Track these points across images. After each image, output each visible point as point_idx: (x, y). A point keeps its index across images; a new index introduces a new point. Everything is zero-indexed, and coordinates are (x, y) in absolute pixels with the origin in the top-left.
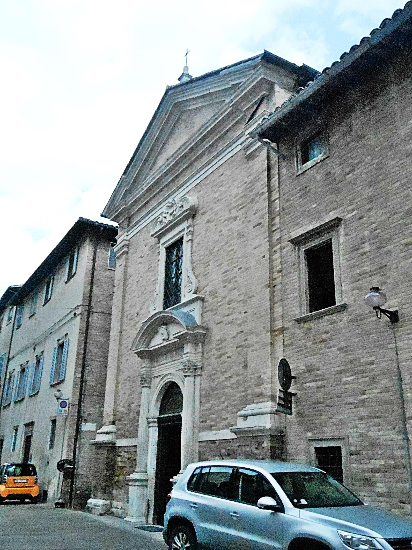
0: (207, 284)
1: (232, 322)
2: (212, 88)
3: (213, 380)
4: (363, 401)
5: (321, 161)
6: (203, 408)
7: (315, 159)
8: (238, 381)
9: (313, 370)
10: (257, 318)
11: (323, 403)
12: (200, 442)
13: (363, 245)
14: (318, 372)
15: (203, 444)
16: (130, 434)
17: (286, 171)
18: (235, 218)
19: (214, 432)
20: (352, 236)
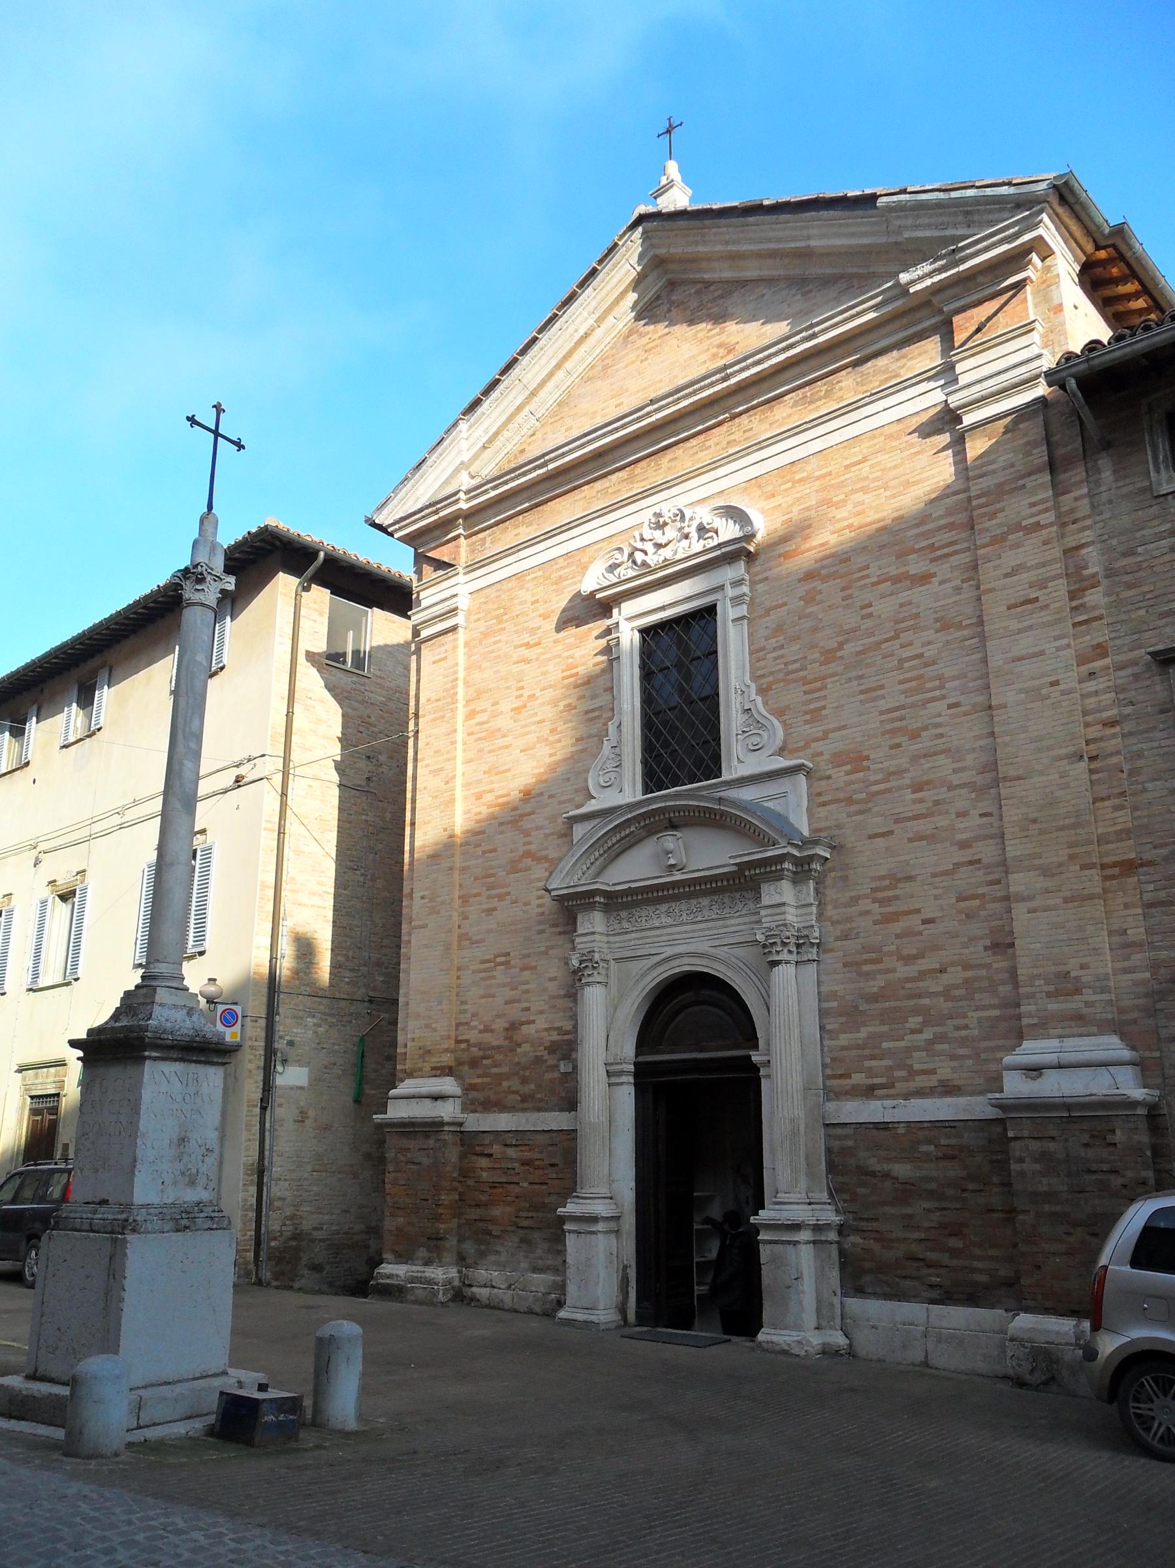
1: (933, 835)
10: (1042, 832)
16: (523, 1101)
17: (1111, 478)
18: (925, 579)
19: (888, 1103)
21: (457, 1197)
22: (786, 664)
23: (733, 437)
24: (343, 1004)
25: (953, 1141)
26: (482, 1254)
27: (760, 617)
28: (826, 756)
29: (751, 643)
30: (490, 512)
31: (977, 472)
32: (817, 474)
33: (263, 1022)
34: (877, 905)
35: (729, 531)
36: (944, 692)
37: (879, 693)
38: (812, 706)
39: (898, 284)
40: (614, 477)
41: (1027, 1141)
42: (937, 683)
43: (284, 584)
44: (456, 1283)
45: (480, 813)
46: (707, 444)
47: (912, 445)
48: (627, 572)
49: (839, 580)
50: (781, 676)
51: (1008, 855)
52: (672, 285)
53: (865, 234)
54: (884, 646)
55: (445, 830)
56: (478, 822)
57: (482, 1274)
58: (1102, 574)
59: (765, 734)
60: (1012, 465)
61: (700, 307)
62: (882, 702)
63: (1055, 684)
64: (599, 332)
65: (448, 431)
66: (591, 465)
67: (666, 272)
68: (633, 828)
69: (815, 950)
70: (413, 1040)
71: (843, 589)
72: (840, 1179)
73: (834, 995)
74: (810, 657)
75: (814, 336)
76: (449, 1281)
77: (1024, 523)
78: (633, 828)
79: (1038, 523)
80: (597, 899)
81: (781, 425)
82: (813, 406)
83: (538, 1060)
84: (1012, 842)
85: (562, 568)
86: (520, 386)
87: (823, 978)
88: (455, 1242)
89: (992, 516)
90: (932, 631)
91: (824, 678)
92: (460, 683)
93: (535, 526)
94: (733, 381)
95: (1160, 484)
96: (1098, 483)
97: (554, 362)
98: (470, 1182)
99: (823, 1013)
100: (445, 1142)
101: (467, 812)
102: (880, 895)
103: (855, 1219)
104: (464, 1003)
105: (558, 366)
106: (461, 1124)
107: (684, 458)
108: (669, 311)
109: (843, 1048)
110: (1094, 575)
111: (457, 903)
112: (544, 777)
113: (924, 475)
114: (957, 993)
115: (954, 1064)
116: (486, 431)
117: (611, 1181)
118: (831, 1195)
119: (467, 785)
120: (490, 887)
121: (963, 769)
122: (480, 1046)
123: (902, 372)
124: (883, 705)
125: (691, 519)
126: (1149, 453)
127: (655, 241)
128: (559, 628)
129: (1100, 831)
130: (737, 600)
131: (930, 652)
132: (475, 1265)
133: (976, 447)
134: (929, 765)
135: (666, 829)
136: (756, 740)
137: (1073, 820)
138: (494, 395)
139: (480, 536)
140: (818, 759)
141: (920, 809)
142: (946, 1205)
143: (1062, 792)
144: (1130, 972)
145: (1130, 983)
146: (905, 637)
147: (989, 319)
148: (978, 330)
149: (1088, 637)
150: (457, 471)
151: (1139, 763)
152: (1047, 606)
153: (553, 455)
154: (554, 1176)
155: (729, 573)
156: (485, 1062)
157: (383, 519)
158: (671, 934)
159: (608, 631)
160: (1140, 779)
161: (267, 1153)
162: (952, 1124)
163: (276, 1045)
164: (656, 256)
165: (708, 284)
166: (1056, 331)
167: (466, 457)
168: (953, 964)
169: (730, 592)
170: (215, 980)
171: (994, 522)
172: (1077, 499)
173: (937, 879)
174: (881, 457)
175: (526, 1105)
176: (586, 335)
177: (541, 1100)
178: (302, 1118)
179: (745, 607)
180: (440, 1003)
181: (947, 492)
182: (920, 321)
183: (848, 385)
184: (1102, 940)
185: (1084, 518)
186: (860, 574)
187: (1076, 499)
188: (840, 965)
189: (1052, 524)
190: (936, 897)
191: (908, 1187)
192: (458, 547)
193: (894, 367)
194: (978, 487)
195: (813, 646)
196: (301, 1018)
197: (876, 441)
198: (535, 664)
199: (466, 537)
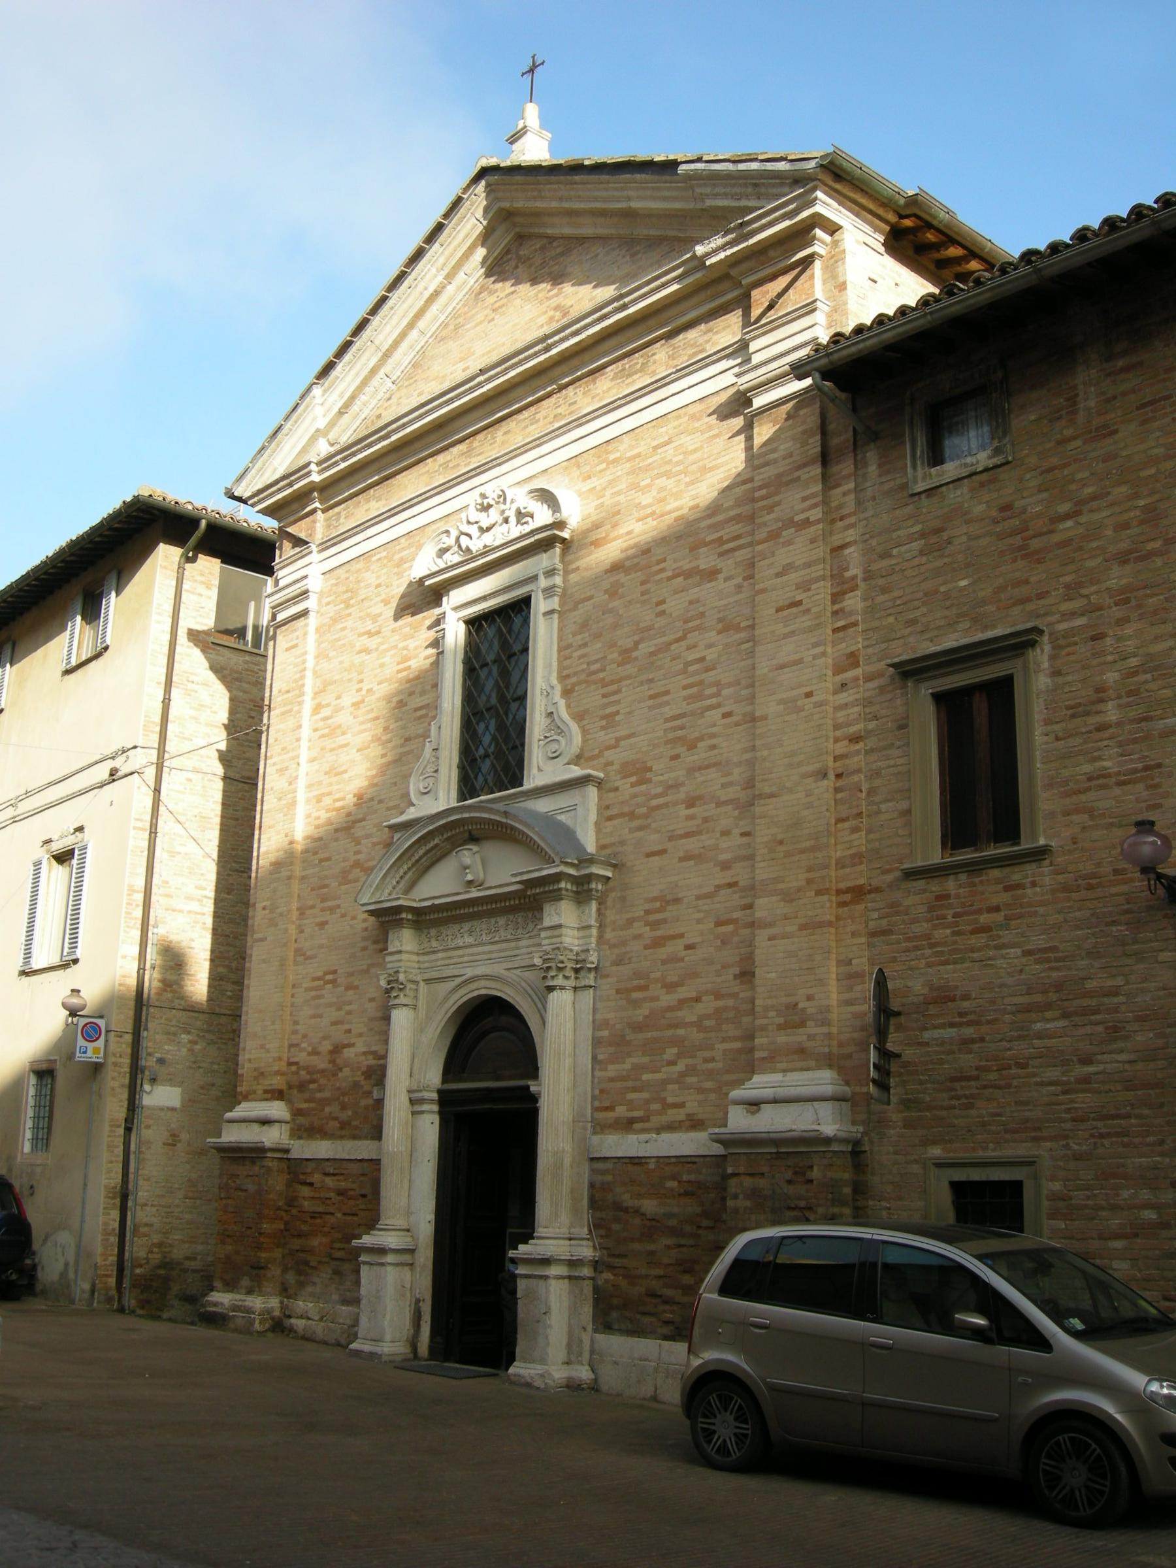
0: (613, 742)
2: (640, 198)
3: (635, 1004)
4: (1086, 1080)
5: (986, 470)
6: (603, 1073)
7: (969, 460)
8: (718, 1011)
9: (953, 1000)
10: (788, 855)
11: (977, 1078)
12: (592, 1159)
13: (1100, 707)
14: (966, 1004)
15: (601, 1166)
16: (342, 1128)
18: (711, 574)
19: (644, 1137)
20: (1070, 678)
21: (282, 1227)
22: (588, 664)
23: (559, 410)
24: (223, 1020)
25: (693, 1177)
26: (301, 1285)
27: (570, 610)
28: (616, 767)
29: (560, 639)
30: (343, 484)
31: (762, 461)
32: (629, 454)
33: (128, 1038)
34: (648, 928)
35: (543, 516)
36: (720, 699)
37: (665, 698)
38: (608, 711)
39: (694, 257)
40: (455, 450)
41: (742, 1177)
42: (714, 690)
43: (166, 555)
44: (277, 1313)
45: (318, 818)
46: (537, 416)
47: (710, 428)
48: (452, 558)
49: (639, 573)
50: (583, 677)
51: (758, 878)
52: (521, 238)
53: (675, 199)
54: (673, 647)
55: (286, 836)
56: (317, 827)
57: (300, 1305)
58: (860, 576)
59: (563, 741)
60: (791, 455)
61: (544, 264)
62: (666, 709)
63: (809, 695)
64: (450, 289)
65: (303, 397)
66: (432, 437)
67: (515, 225)
68: (437, 841)
69: (592, 975)
70: (250, 1060)
71: (643, 583)
72: (598, 1214)
73: (605, 1024)
74: (609, 657)
75: (624, 307)
76: (268, 1311)
77: (796, 519)
78: (437, 841)
79: (808, 519)
80: (404, 915)
81: (601, 400)
82: (630, 380)
83: (356, 1085)
84: (762, 864)
85: (403, 549)
86: (373, 348)
87: (599, 1005)
88: (278, 1272)
89: (770, 509)
90: (714, 633)
91: (620, 681)
92: (309, 674)
93: (384, 502)
94: (554, 351)
95: (916, 482)
96: (865, 476)
97: (405, 322)
98: (294, 1212)
99: (596, 1042)
100: (269, 1170)
101: (309, 816)
102: (652, 917)
103: (610, 1256)
104: (296, 1023)
105: (411, 325)
106: (287, 1151)
107: (516, 432)
108: (517, 267)
109: (612, 1080)
110: (854, 578)
111: (295, 914)
112: (375, 781)
113: (720, 461)
114: (708, 1023)
115: (701, 1097)
116: (341, 395)
117: (409, 1213)
118: (590, 1232)
119: (309, 786)
120: (324, 900)
121: (731, 784)
122: (306, 1068)
123: (708, 346)
124: (668, 711)
125: (512, 501)
126: (908, 446)
127: (500, 195)
128: (398, 616)
129: (839, 854)
130: (549, 591)
131: (711, 655)
132: (294, 1297)
133: (763, 432)
134: (702, 779)
135: (465, 843)
136: (554, 746)
137: (812, 843)
138: (348, 357)
139: (337, 510)
140: (609, 768)
141: (691, 825)
142: (683, 1242)
143: (806, 813)
144: (852, 1005)
145: (849, 1016)
146: (692, 638)
147: (780, 295)
148: (771, 307)
149: (844, 645)
150: (313, 439)
151: (878, 782)
152: (808, 610)
153: (394, 426)
154: (363, 1207)
155: (544, 560)
156: (312, 1086)
157: (241, 491)
158: (472, 955)
159: (438, 622)
160: (877, 799)
161: (131, 1176)
162: (694, 1159)
163: (143, 1063)
164: (501, 210)
165: (552, 239)
166: (838, 309)
167: (322, 424)
168: (707, 993)
169: (543, 582)
170: (79, 991)
171: (772, 516)
172: (844, 495)
173: (700, 902)
174: (684, 439)
175: (343, 1133)
176: (437, 294)
177: (356, 1128)
178: (173, 1141)
179: (556, 599)
180: (273, 1023)
181: (740, 481)
182: (724, 293)
183: (661, 358)
184: (832, 971)
185: (849, 515)
186: (658, 567)
187: (844, 494)
188: (614, 992)
189: (818, 521)
190: (699, 921)
191: (654, 1223)
192: (314, 522)
193: (701, 341)
194: (761, 477)
195: (613, 645)
196: (174, 1034)
197: (681, 421)
198: (375, 654)
199: (324, 511)
